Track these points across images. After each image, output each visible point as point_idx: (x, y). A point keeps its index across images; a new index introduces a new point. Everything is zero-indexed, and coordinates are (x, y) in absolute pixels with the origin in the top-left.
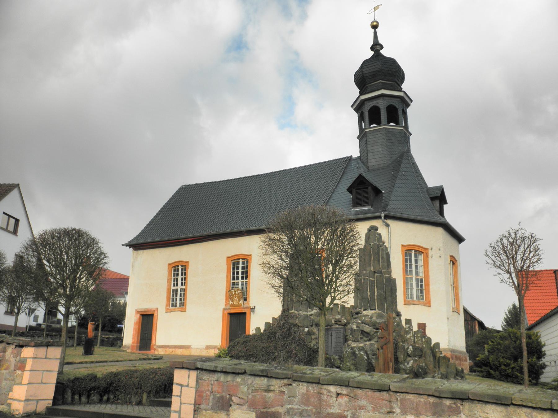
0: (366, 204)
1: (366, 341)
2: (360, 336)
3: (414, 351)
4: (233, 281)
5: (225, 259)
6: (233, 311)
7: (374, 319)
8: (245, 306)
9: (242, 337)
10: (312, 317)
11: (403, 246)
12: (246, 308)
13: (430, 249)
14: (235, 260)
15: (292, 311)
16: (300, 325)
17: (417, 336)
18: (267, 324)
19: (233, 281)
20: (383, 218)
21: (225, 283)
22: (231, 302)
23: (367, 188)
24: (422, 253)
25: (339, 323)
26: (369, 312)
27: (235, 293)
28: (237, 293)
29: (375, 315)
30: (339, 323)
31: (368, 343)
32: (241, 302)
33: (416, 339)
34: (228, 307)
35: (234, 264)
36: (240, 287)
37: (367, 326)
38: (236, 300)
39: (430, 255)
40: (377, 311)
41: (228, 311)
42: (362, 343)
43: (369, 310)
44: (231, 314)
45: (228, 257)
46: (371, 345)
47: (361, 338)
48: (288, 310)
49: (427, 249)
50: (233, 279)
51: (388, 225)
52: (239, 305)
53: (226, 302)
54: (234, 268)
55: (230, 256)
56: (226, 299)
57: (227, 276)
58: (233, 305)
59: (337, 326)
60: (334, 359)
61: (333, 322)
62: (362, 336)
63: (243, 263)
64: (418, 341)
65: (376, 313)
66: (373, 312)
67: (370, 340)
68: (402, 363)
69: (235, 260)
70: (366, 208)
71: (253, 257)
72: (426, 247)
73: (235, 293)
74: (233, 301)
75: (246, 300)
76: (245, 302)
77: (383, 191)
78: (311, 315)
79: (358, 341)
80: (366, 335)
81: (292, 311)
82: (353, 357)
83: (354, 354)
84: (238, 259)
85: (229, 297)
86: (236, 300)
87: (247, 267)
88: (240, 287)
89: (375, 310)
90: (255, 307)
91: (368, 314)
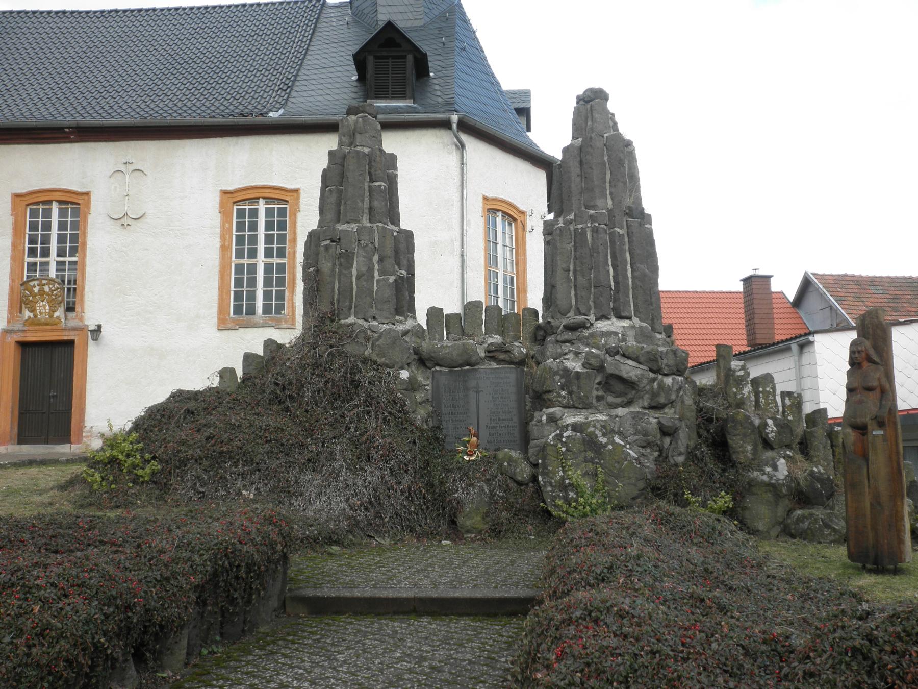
0: (402, 95)
1: (615, 406)
2: (595, 393)
3: (779, 433)
4: (32, 260)
5: (8, 199)
6: (31, 338)
7: (632, 342)
8: (71, 324)
9: (647, 347)
10: (407, 339)
11: (485, 199)
12: (74, 329)
13: (528, 214)
14: (37, 203)
15: (351, 320)
16: (381, 360)
17: (764, 392)
18: (249, 358)
19: (32, 260)
20: (455, 126)
21: (7, 262)
22: (27, 314)
23: (404, 57)
24: (515, 220)
25: (502, 356)
26: (615, 325)
27: (41, 292)
28: (46, 289)
29: (631, 333)
30: (502, 356)
31: (621, 411)
32: (59, 313)
33: (762, 400)
34: (18, 326)
35: (34, 214)
36: (53, 273)
37: (630, 362)
38: (43, 307)
39: (529, 228)
40: (636, 321)
41: (20, 337)
42: (601, 412)
43: (614, 319)
44: (24, 345)
45: (17, 196)
46: (636, 416)
47: (599, 398)
48: (334, 316)
49: (523, 213)
50: (32, 252)
51: (461, 146)
52: (52, 323)
53: (10, 312)
54: (34, 226)
55: (24, 191)
56: (11, 306)
57: (14, 246)
58: (33, 322)
59: (494, 365)
60: (510, 460)
61: (483, 355)
62: (600, 393)
63: (62, 213)
64: (767, 404)
65: (633, 327)
66: (626, 323)
67: (629, 403)
68: (749, 467)
69: (37, 203)
70: (401, 104)
71: (93, 197)
72: (522, 208)
73: (41, 292)
74: (32, 310)
75: (70, 309)
76: (70, 315)
77: (432, 74)
78: (406, 333)
79: (587, 406)
80: (619, 387)
81: (351, 320)
82: (590, 454)
83: (591, 443)
84: (49, 202)
85: (21, 299)
86: (43, 307)
87: (75, 225)
88: (53, 273)
89: (630, 318)
90: (99, 327)
91: (613, 329)
